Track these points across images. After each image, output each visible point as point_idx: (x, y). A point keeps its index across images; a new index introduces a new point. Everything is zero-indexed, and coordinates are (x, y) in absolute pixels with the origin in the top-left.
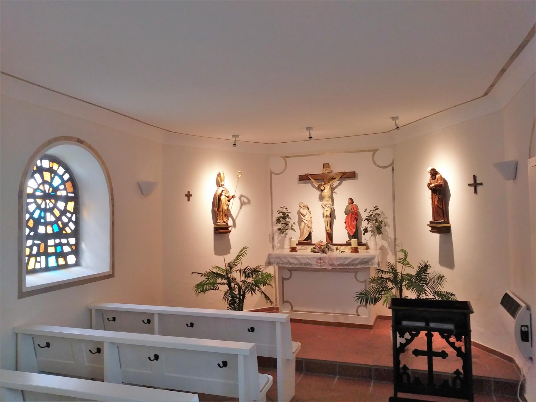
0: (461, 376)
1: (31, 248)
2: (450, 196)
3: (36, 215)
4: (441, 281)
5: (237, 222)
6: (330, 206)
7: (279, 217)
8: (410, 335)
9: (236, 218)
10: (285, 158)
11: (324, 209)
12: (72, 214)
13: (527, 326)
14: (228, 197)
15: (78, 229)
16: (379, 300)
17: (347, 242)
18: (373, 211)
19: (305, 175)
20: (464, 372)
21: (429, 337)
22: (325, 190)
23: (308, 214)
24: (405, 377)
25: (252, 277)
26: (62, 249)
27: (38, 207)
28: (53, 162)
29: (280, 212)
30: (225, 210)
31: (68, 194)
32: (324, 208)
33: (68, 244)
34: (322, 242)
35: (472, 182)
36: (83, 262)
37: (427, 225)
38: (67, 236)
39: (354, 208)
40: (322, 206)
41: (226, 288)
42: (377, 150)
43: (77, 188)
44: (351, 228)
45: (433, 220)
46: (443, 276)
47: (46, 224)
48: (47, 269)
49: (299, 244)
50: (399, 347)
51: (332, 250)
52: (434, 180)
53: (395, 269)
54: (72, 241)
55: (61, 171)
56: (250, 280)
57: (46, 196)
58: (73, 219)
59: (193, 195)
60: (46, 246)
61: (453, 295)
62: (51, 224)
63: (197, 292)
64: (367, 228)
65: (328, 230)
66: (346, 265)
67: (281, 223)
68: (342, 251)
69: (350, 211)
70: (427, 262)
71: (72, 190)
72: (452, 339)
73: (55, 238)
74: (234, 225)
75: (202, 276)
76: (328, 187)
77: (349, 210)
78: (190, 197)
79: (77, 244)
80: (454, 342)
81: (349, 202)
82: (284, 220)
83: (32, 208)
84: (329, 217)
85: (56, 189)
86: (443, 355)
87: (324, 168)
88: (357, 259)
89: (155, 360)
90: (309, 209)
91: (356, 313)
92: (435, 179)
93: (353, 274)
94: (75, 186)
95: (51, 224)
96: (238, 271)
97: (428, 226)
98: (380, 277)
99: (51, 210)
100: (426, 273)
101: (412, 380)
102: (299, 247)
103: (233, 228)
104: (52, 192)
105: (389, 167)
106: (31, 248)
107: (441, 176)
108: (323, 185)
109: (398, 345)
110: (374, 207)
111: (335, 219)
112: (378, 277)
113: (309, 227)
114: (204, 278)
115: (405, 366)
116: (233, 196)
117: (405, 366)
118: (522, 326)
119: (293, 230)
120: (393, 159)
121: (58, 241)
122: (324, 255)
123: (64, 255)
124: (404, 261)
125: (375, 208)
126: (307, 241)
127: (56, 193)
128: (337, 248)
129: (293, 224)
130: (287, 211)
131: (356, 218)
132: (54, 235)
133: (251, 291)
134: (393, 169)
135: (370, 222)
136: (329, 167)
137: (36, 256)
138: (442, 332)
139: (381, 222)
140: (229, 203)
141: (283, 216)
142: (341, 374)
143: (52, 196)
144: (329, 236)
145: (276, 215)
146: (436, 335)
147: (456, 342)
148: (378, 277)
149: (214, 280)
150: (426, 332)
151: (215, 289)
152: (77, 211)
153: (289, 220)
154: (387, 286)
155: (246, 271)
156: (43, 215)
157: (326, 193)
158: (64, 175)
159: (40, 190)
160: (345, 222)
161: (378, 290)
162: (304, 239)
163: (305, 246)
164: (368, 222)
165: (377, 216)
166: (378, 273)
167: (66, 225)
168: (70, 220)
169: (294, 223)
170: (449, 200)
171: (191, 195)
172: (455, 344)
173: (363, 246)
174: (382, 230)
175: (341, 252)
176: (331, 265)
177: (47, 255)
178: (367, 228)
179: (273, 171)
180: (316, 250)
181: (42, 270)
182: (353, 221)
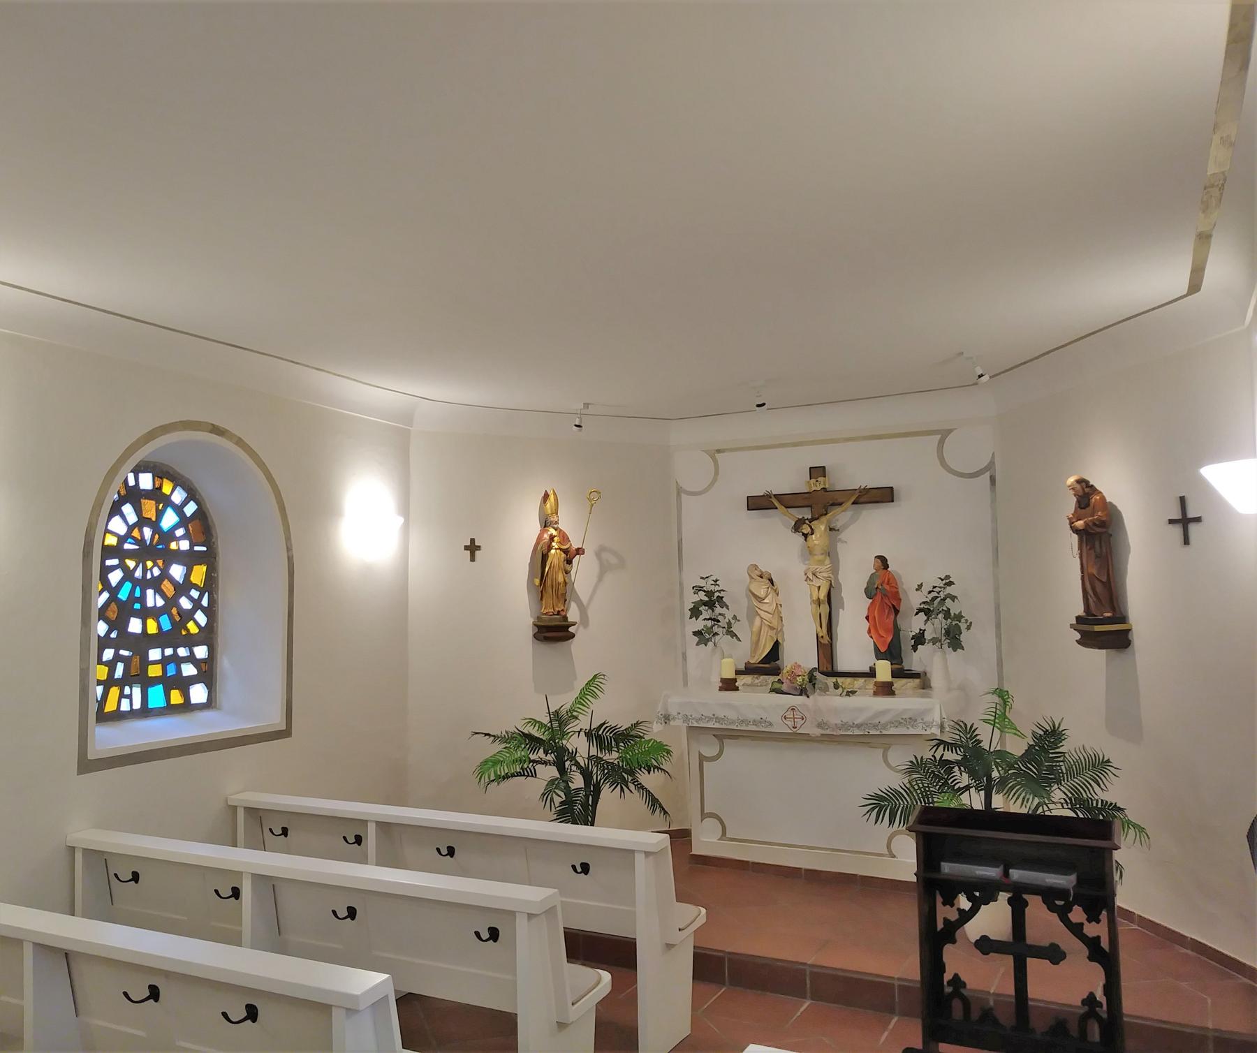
1: (111, 665)
2: (1129, 552)
3: (123, 595)
4: (1100, 775)
5: (590, 613)
6: (825, 574)
8: (969, 901)
11: (811, 583)
14: (566, 552)
17: (870, 668)
21: (1018, 907)
22: (812, 534)
23: (770, 596)
24: (957, 1005)
25: (616, 749)
26: (179, 671)
27: (128, 575)
28: (161, 478)
29: (698, 589)
30: (559, 584)
33: (191, 659)
34: (800, 666)
35: (1177, 515)
36: (221, 697)
38: (191, 642)
39: (888, 581)
40: (806, 574)
41: (553, 772)
42: (950, 431)
43: (214, 534)
44: (882, 633)
45: (1084, 614)
46: (1105, 759)
47: (145, 614)
48: (145, 712)
49: (750, 670)
50: (942, 929)
51: (825, 690)
52: (1084, 508)
54: (201, 652)
55: (178, 497)
56: (613, 757)
57: (145, 552)
58: (205, 602)
59: (482, 548)
60: (145, 663)
62: (155, 613)
63: (480, 779)
64: (922, 632)
66: (859, 726)
67: (702, 617)
68: (849, 690)
69: (877, 588)
70: (1059, 724)
72: (1077, 915)
74: (585, 621)
76: (820, 527)
77: (876, 586)
78: (477, 552)
79: (210, 662)
80: (1082, 924)
83: (115, 577)
84: (824, 604)
85: (169, 536)
86: (1054, 954)
88: (884, 712)
89: (349, 919)
90: (773, 584)
91: (886, 850)
92: (1088, 505)
93: (880, 751)
95: (155, 613)
96: (582, 734)
98: (938, 758)
99: (156, 584)
100: (1057, 750)
101: (975, 1015)
103: (581, 628)
104: (158, 544)
105: (983, 473)
106: (111, 665)
107: (1103, 498)
108: (807, 522)
109: (940, 926)
110: (942, 580)
112: (933, 759)
113: (772, 628)
114: (498, 747)
115: (956, 977)
116: (579, 549)
117: (956, 977)
119: (733, 635)
121: (169, 652)
122: (802, 699)
123: (184, 685)
124: (1000, 719)
125: (944, 582)
126: (770, 664)
128: (837, 682)
129: (733, 621)
130: (717, 588)
132: (161, 639)
133: (619, 786)
134: (993, 480)
136: (825, 477)
137: (121, 683)
138: (1049, 895)
140: (568, 567)
141: (706, 599)
142: (816, 996)
143: (159, 550)
144: (826, 649)
145: (691, 598)
147: (1086, 923)
148: (933, 759)
149: (523, 753)
151: (526, 774)
152: (210, 585)
153: (724, 611)
154: (954, 783)
155: (600, 733)
156: (138, 593)
157: (816, 542)
158: (185, 505)
159: (133, 538)
160: (867, 618)
161: (926, 791)
162: (760, 659)
164: (925, 618)
166: (935, 748)
167: (189, 615)
168: (197, 604)
169: (735, 617)
171: (479, 548)
172: (1082, 929)
173: (911, 680)
174: (962, 638)
175: (844, 693)
176: (819, 726)
177: (147, 683)
178: (922, 632)
180: (784, 687)
181: (132, 714)
182: (885, 617)
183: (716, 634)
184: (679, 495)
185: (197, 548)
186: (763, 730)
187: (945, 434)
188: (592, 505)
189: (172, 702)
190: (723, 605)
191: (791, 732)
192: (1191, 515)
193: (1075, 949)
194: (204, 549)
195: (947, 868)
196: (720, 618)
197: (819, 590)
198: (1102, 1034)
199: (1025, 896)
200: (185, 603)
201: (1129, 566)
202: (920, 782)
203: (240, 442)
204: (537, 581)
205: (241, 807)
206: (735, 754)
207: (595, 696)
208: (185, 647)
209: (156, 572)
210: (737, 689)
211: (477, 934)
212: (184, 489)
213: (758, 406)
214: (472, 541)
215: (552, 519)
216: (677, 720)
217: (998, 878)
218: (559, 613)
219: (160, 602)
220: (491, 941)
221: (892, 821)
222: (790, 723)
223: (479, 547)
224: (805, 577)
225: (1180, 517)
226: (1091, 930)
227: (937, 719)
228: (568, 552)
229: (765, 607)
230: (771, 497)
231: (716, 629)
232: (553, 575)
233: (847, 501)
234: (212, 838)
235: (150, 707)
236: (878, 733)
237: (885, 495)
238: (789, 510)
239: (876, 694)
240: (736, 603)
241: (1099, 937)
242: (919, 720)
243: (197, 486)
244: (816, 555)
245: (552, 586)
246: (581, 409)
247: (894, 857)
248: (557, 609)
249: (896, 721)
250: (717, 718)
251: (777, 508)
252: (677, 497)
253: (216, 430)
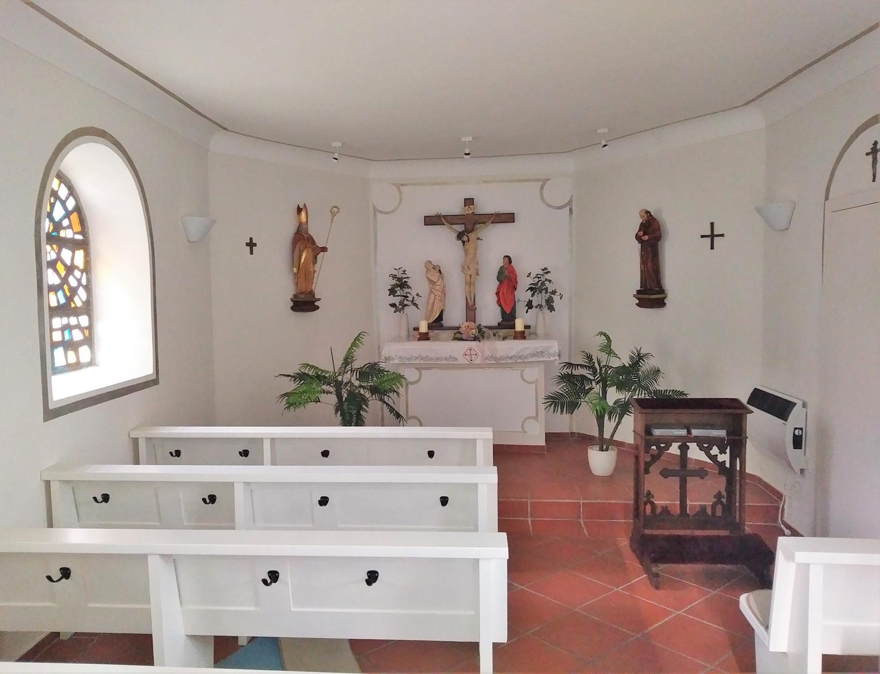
0: (722, 499)
7: (392, 285)
10: (399, 186)
12: (82, 271)
13: (801, 429)
15: (91, 299)
16: (579, 407)
17: (498, 323)
18: (540, 276)
31: (75, 235)
36: (100, 357)
38: (76, 312)
53: (344, 383)
54: (84, 320)
58: (84, 282)
66: (511, 358)
69: (506, 275)
71: (79, 229)
72: (715, 451)
75: (291, 379)
79: (90, 328)
80: (717, 455)
82: (401, 290)
87: (465, 206)
94: (82, 221)
101: (659, 510)
104: (53, 231)
110: (543, 270)
118: (795, 429)
119: (415, 305)
120: (572, 196)
121: (65, 320)
124: (608, 349)
127: (59, 233)
130: (405, 276)
134: (571, 210)
135: (536, 294)
138: (701, 442)
139: (554, 292)
146: (693, 446)
147: (719, 454)
167: (74, 291)
169: (418, 295)
171: (255, 245)
180: (464, 337)
187: (545, 181)
195: (657, 432)
196: (408, 295)
197: (471, 277)
200: (73, 282)
205: (142, 438)
207: (358, 347)
214: (251, 239)
222: (468, 358)
223: (256, 244)
226: (721, 458)
230: (440, 217)
231: (406, 302)
233: (488, 221)
236: (522, 361)
237: (509, 218)
238: (453, 226)
239: (419, 339)
242: (546, 353)
249: (533, 354)
250: (421, 357)
251: (444, 225)
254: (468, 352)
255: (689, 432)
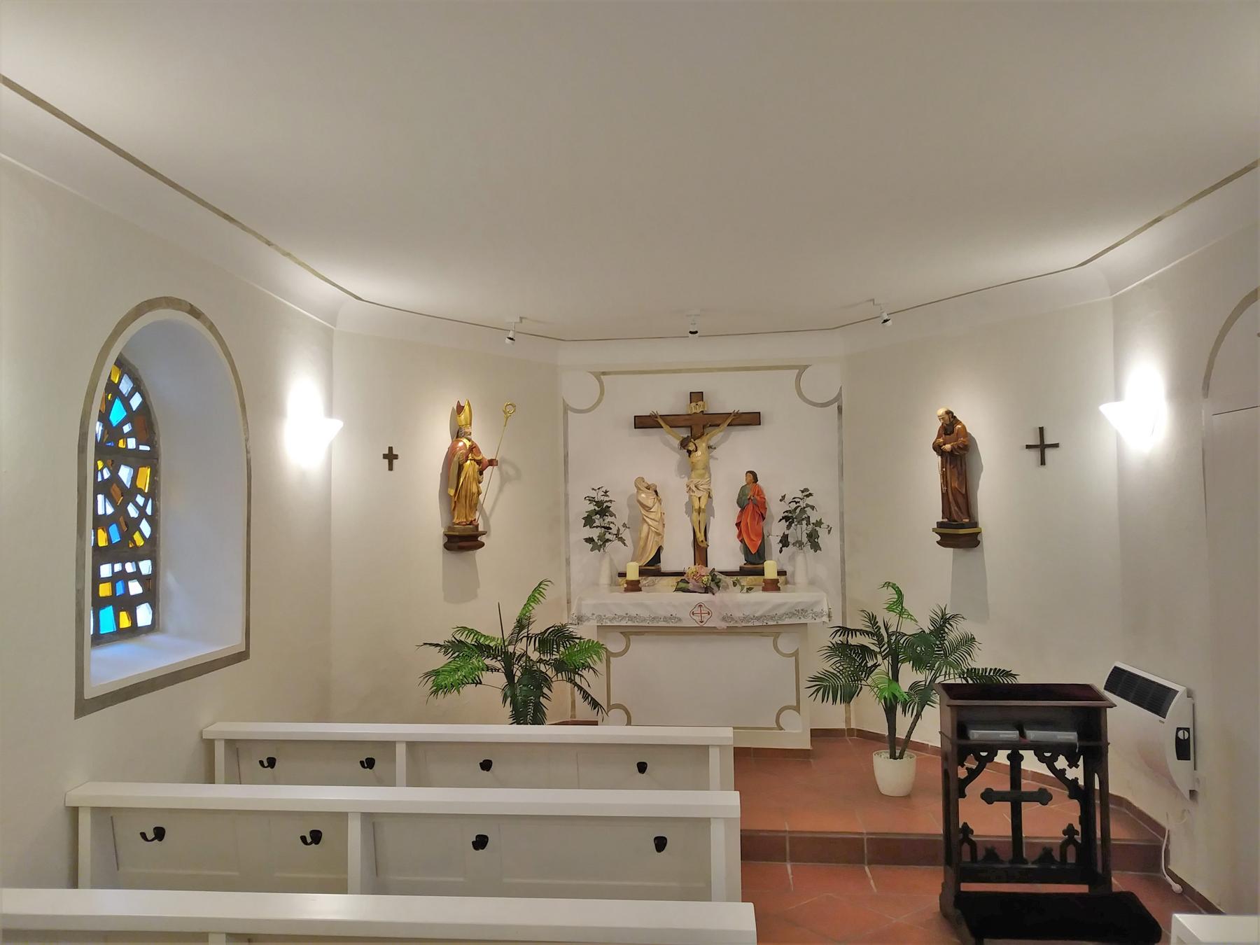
2: (982, 471)
9: (491, 515)
10: (599, 375)
12: (147, 497)
13: (1187, 730)
14: (479, 462)
15: (157, 536)
17: (740, 567)
19: (650, 416)
20: (971, 840)
22: (696, 451)
23: (656, 505)
26: (126, 588)
30: (473, 494)
32: (693, 491)
36: (165, 619)
37: (931, 530)
42: (807, 367)
43: (156, 432)
44: (753, 537)
54: (146, 567)
58: (149, 511)
61: (1011, 675)
65: (702, 541)
66: (758, 619)
69: (749, 499)
72: (1061, 763)
73: (113, 562)
76: (702, 445)
78: (395, 461)
80: (1065, 770)
81: (749, 478)
86: (1043, 797)
87: (691, 403)
90: (657, 494)
91: (775, 724)
92: (953, 432)
97: (934, 533)
101: (981, 854)
102: (645, 581)
107: (964, 427)
111: (714, 517)
113: (658, 534)
118: (1179, 729)
119: (621, 540)
120: (841, 388)
121: (118, 567)
125: (804, 494)
131: (762, 514)
134: (840, 409)
139: (819, 523)
147: (1068, 768)
150: (1009, 752)
160: (738, 525)
163: (650, 578)
165: (808, 509)
170: (979, 478)
171: (396, 457)
174: (820, 541)
176: (724, 619)
179: (573, 403)
180: (690, 586)
183: (608, 540)
184: (565, 413)
185: (142, 448)
186: (673, 625)
187: (802, 369)
188: (507, 418)
189: (121, 627)
190: (612, 515)
191: (698, 625)
192: (1047, 442)
193: (1059, 793)
194: (148, 448)
196: (611, 526)
198: (1078, 856)
199: (1021, 752)
201: (981, 482)
202: (839, 664)
203: (212, 328)
204: (452, 492)
206: (642, 650)
208: (131, 562)
209: (106, 474)
210: (640, 590)
211: (143, 835)
212: (130, 378)
213: (691, 333)
214: (391, 449)
215: (467, 430)
216: (591, 621)
217: (1017, 739)
218: (471, 523)
219: (110, 510)
220: (156, 840)
221: (834, 700)
222: (698, 618)
224: (686, 489)
225: (1039, 444)
227: (826, 609)
228: (481, 463)
229: (652, 516)
230: (656, 417)
231: (608, 536)
232: (467, 486)
234: (189, 779)
235: (101, 633)
236: (775, 623)
237: (752, 419)
240: (621, 513)
241: (1077, 779)
243: (143, 377)
244: (697, 469)
245: (466, 496)
246: (515, 323)
247: (782, 729)
248: (470, 519)
249: (790, 613)
252: (564, 414)
253: (194, 312)
254: (697, 610)
255: (1022, 735)
